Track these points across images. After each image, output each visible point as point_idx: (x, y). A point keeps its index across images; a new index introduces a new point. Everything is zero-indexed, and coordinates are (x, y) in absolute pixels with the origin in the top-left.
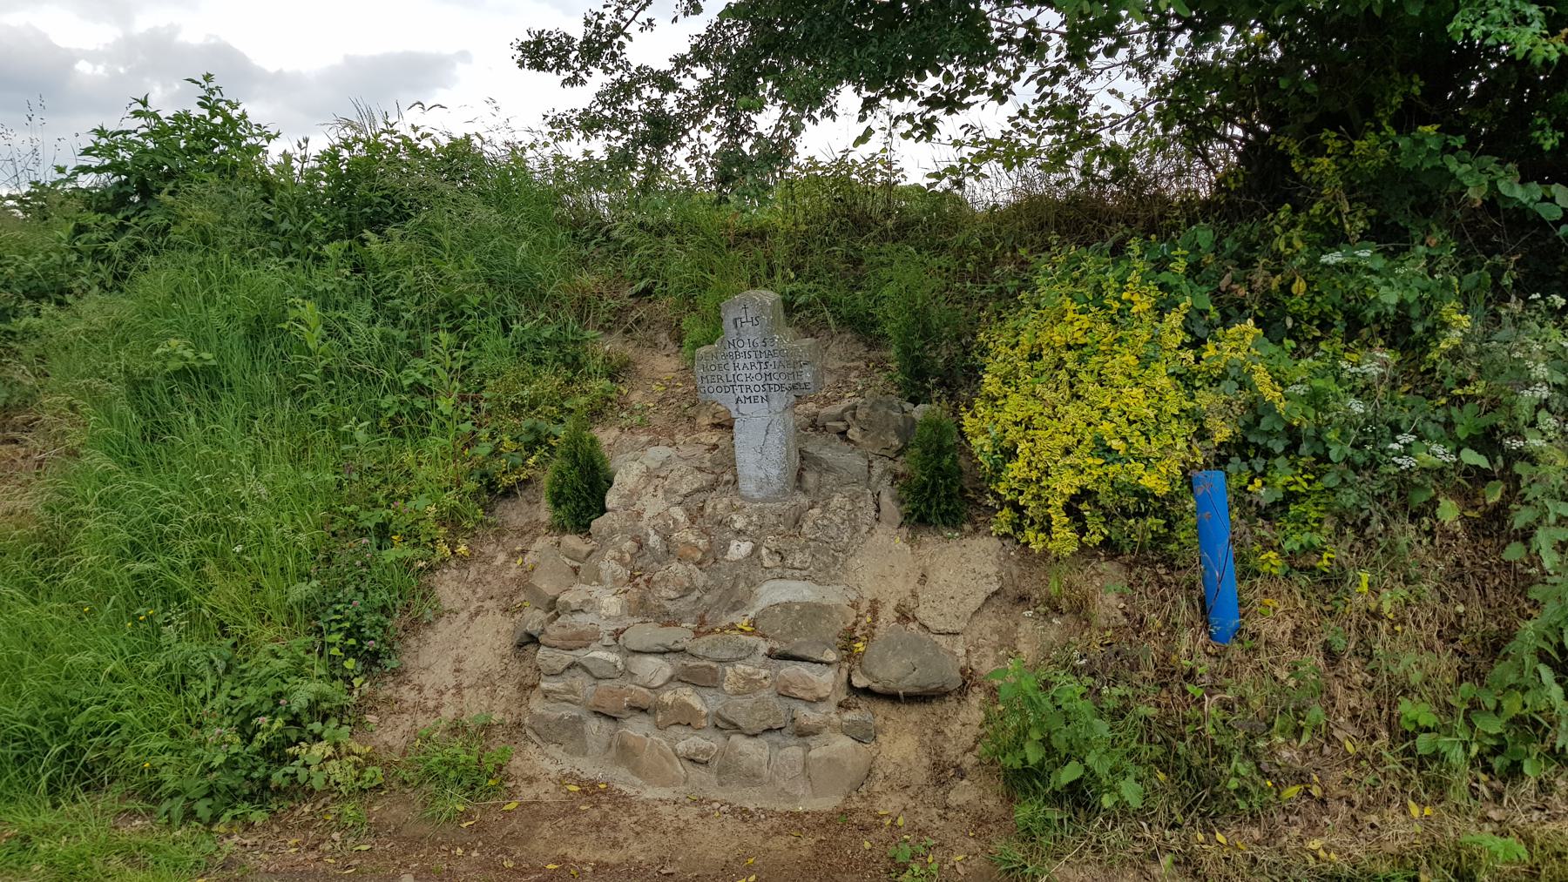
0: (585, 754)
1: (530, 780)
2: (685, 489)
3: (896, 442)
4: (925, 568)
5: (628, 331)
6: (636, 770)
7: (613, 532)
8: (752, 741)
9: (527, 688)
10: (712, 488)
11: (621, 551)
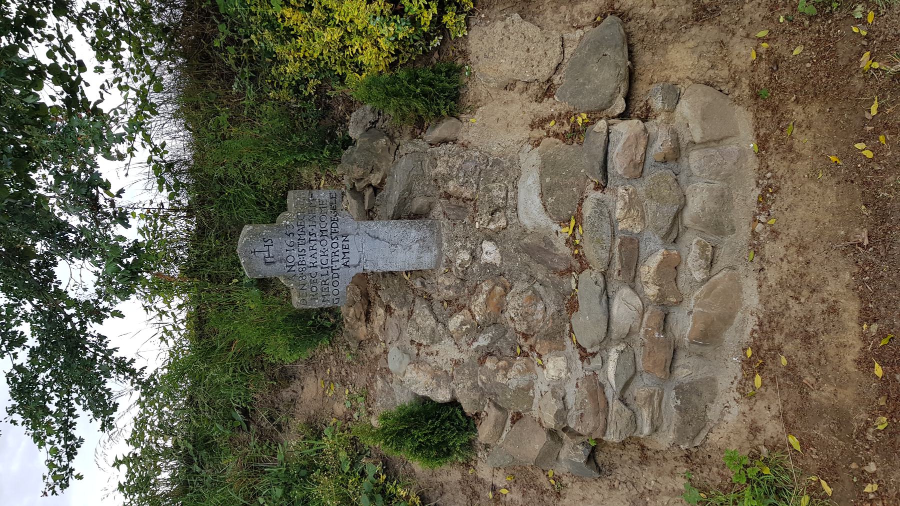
0: (714, 380)
1: (754, 430)
2: (431, 322)
3: (383, 141)
4: (500, 87)
5: (279, 427)
6: (726, 320)
7: (475, 386)
8: (690, 199)
9: (645, 456)
10: (429, 299)
11: (498, 370)
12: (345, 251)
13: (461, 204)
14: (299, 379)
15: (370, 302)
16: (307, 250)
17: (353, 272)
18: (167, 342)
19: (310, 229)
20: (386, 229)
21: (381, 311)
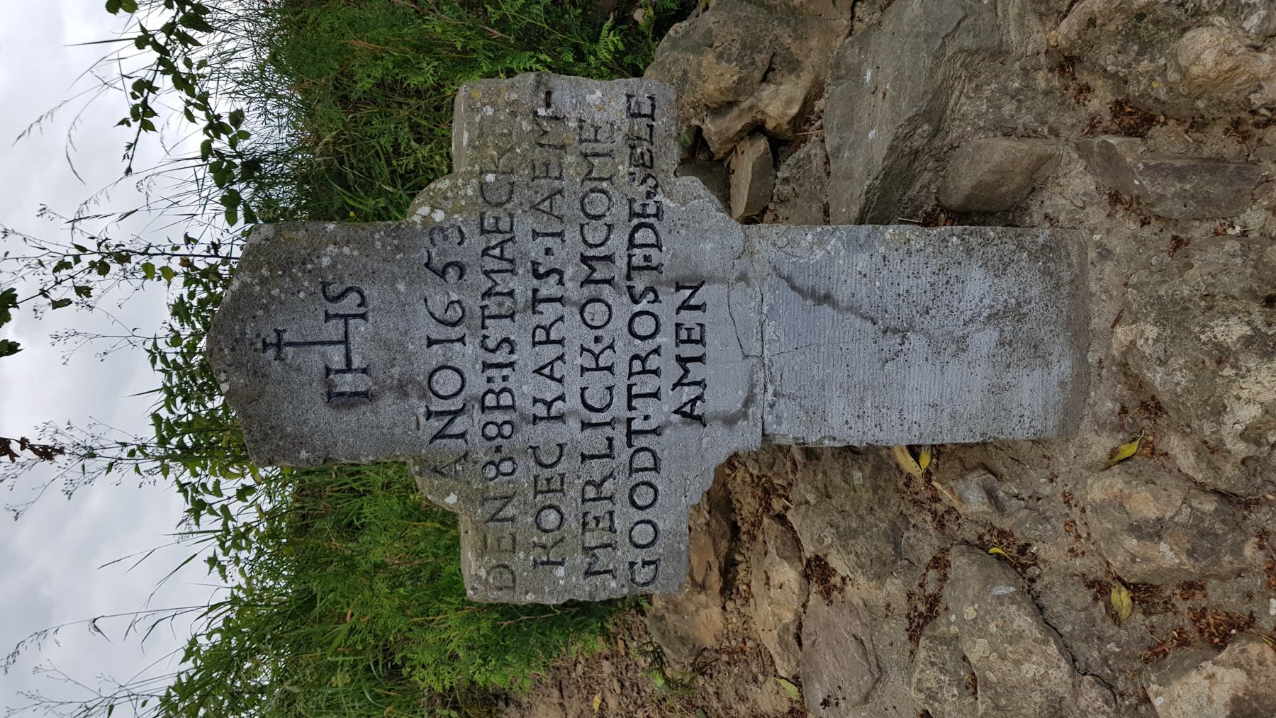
10: (1019, 561)
12: (689, 351)
13: (1218, 142)
14: (519, 705)
15: (735, 529)
16: (523, 342)
17: (719, 444)
18: (222, 569)
19: (535, 249)
20: (862, 261)
21: (787, 574)
